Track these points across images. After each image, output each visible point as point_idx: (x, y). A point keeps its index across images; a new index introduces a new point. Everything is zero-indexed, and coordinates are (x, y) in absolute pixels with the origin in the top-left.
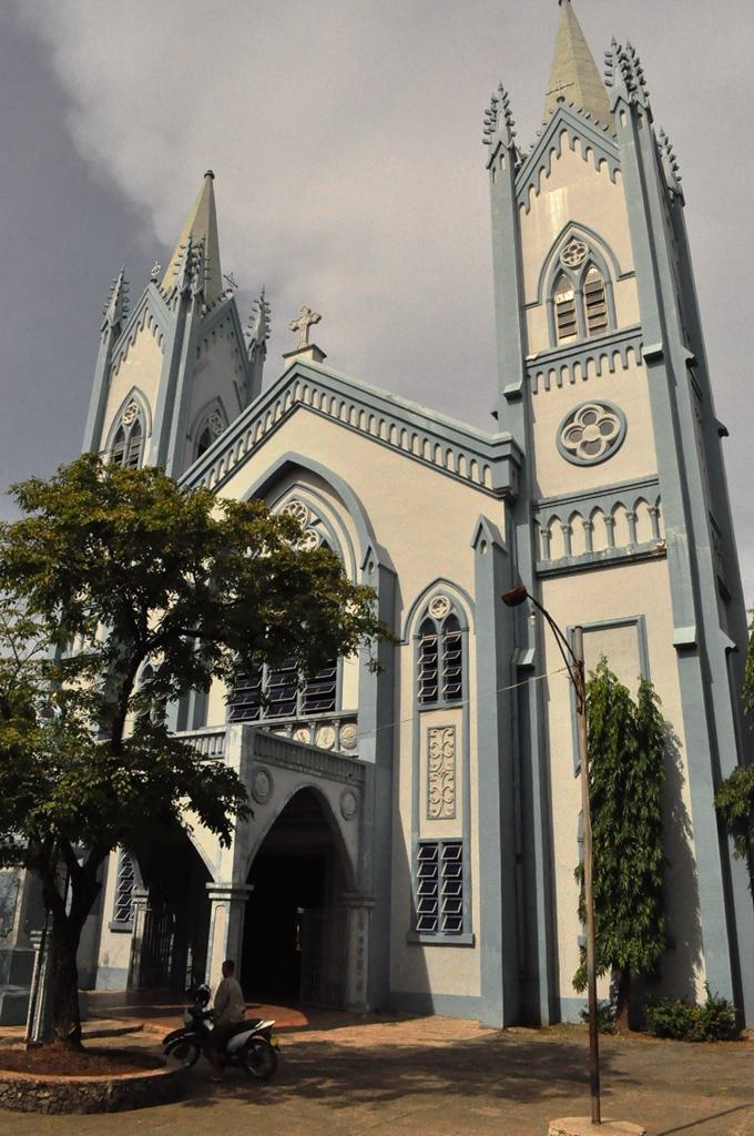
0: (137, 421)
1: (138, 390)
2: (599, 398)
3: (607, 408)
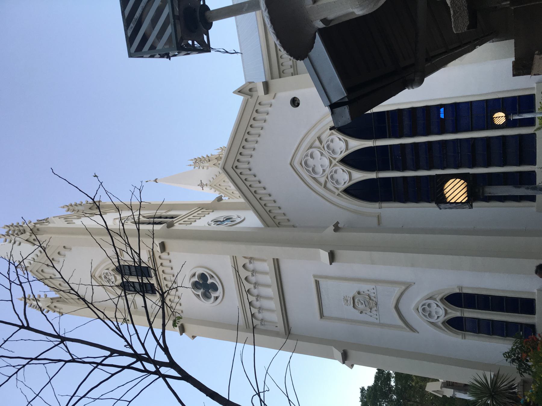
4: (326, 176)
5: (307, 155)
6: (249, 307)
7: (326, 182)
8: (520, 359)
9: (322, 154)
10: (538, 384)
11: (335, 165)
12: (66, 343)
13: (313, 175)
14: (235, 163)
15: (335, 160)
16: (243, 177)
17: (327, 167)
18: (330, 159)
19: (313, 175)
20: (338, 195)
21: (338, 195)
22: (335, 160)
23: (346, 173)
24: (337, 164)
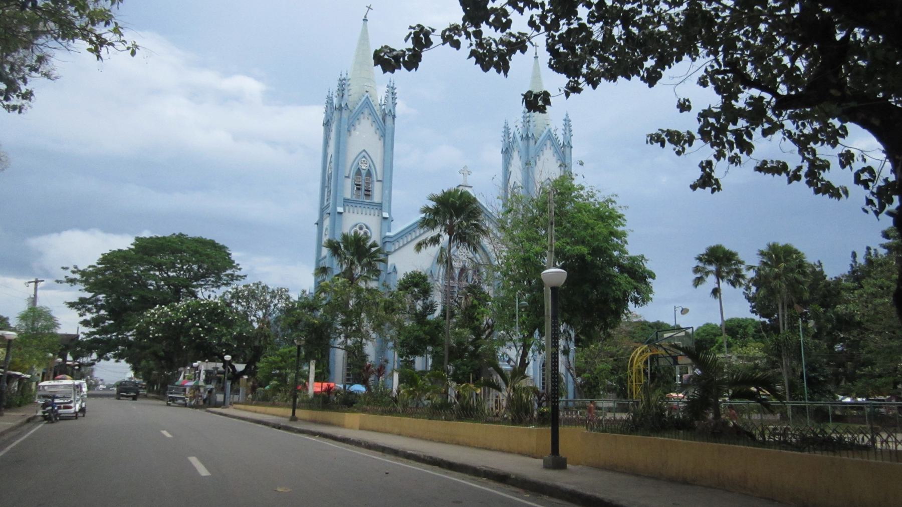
0: (369, 170)
1: (366, 152)
2: (364, 222)
3: (367, 228)
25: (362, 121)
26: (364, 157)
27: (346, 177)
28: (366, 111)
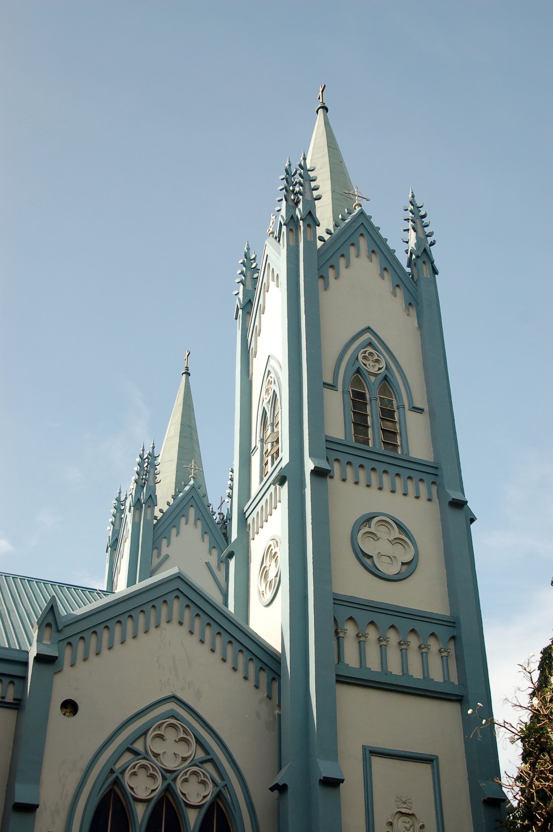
4: (146, 756)
5: (185, 731)
6: (219, 507)
7: (136, 753)
8: (544, 810)
9: (184, 759)
10: (540, 821)
11: (164, 778)
12: (311, 238)
13: (152, 733)
14: (158, 600)
15: (172, 780)
16: (146, 608)
17: (163, 765)
18: (175, 771)
19: (152, 733)
20: (112, 771)
21: (112, 771)
22: (172, 780)
23: (149, 795)
24: (166, 783)
25: (183, 527)
26: (370, 344)
27: (325, 384)
28: (192, 512)
